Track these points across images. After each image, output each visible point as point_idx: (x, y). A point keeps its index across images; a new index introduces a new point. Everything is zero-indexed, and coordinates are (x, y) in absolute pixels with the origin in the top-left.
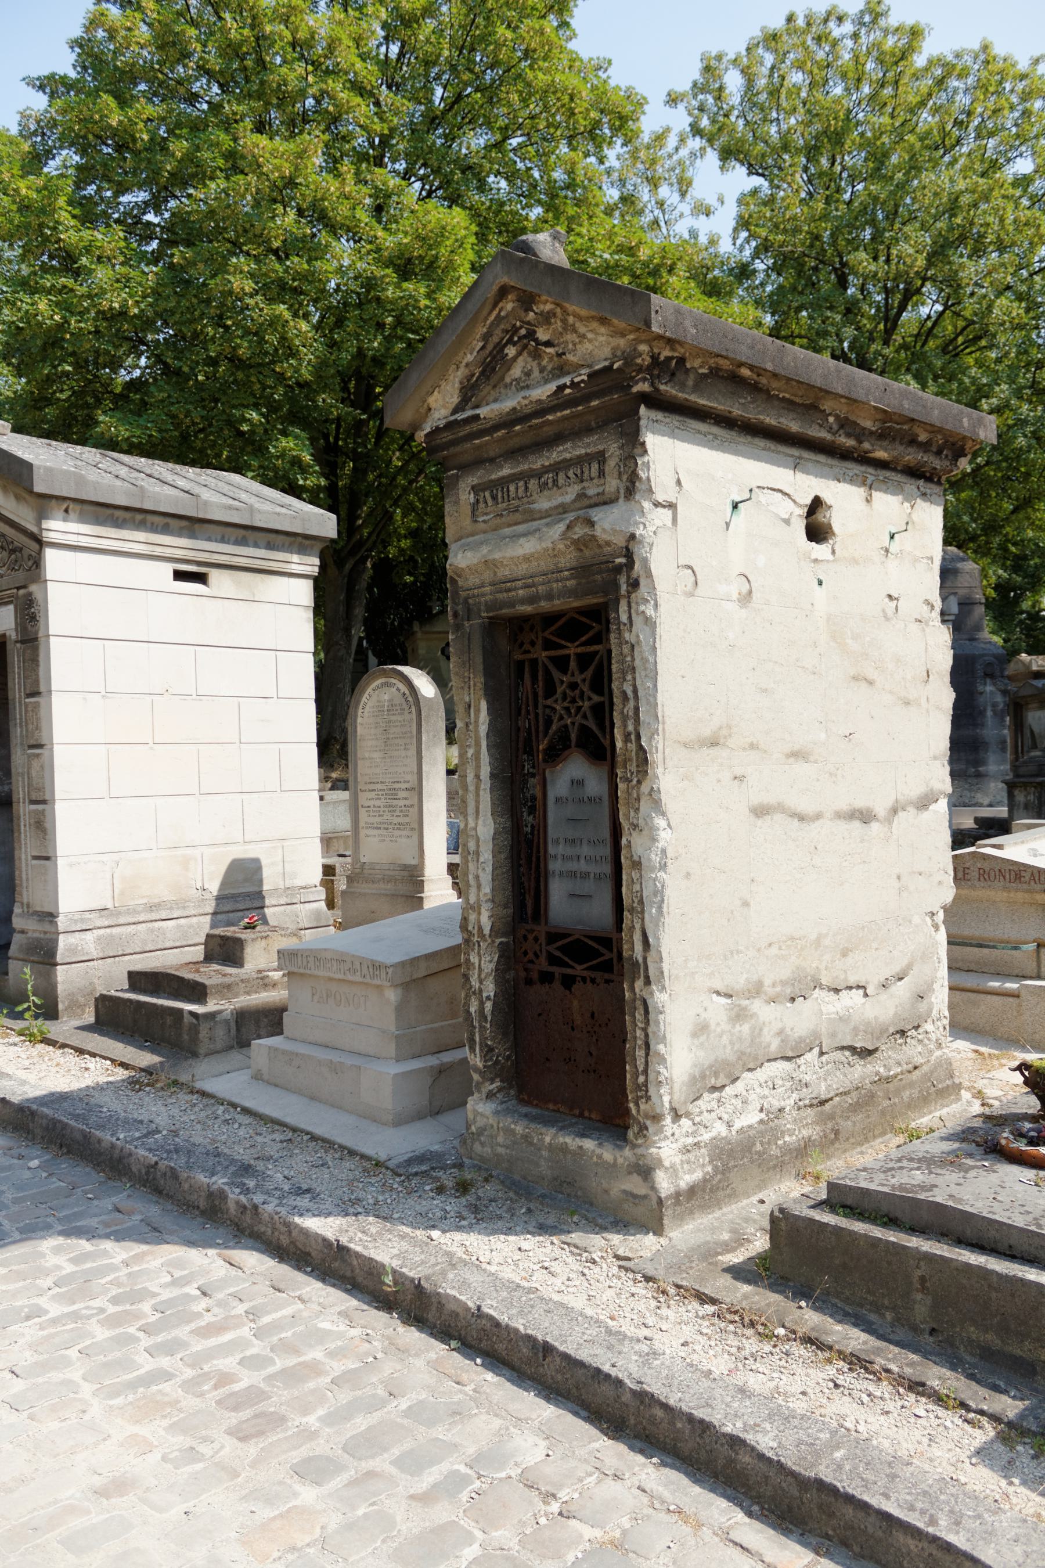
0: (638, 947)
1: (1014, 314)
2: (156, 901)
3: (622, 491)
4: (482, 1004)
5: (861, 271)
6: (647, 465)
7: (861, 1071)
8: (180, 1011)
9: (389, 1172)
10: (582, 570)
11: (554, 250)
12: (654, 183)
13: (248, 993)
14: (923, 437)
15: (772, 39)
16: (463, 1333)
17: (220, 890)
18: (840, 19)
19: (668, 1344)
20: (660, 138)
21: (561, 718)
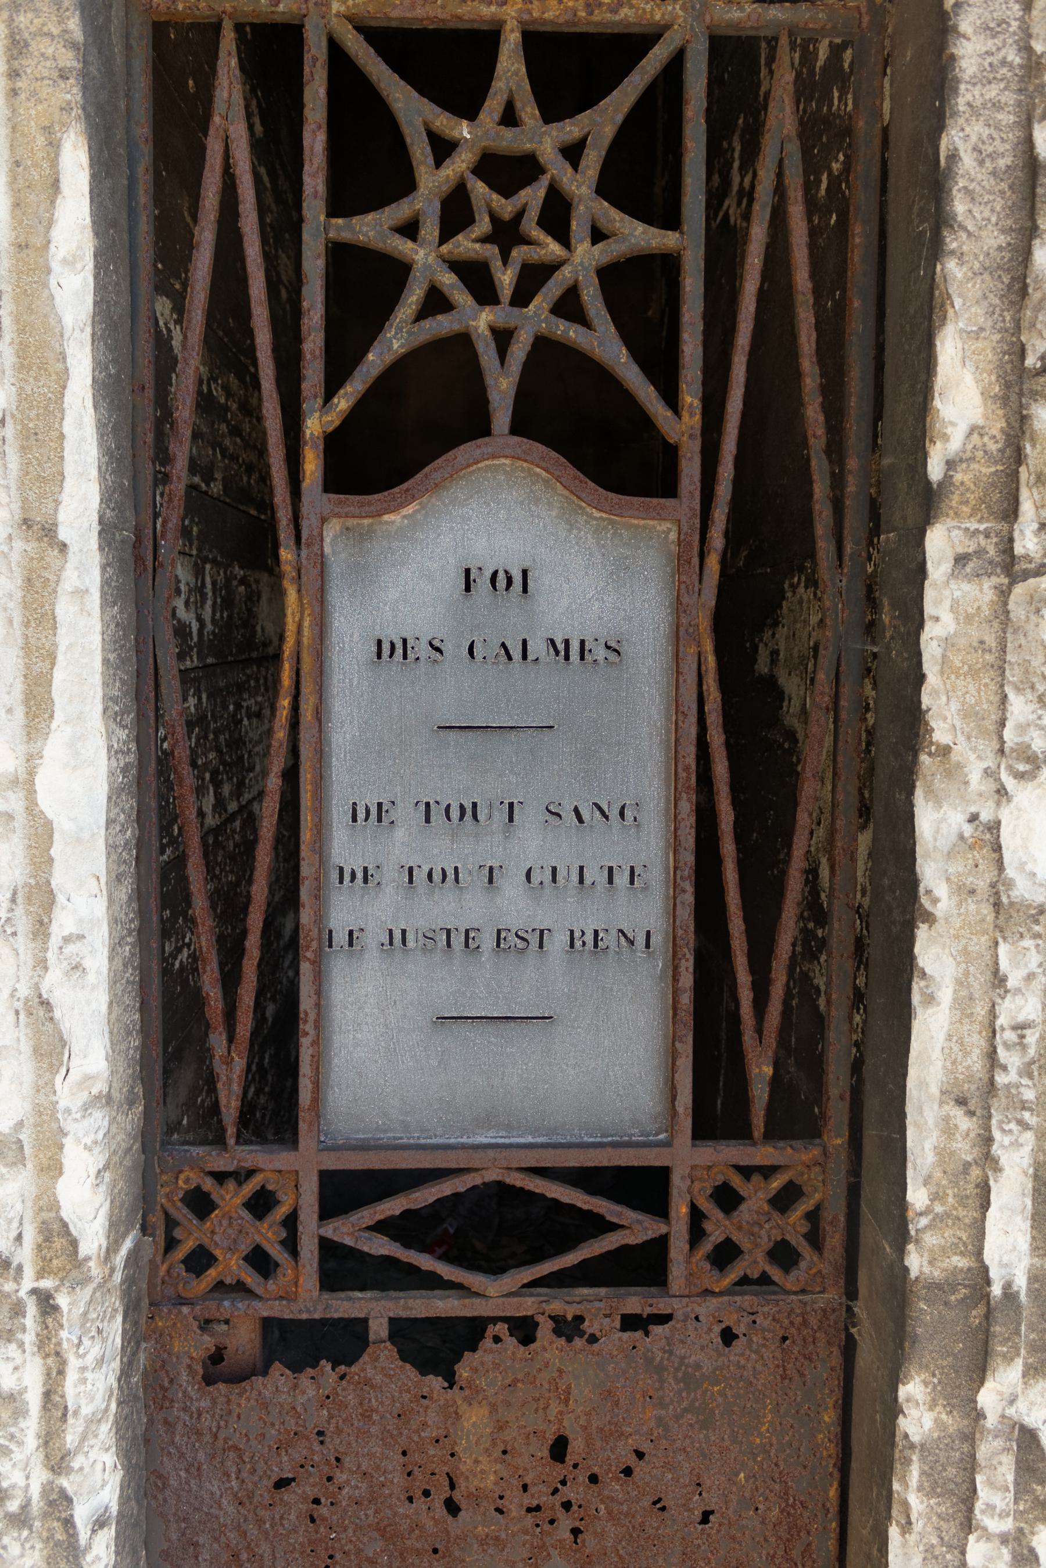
21: (436, 302)
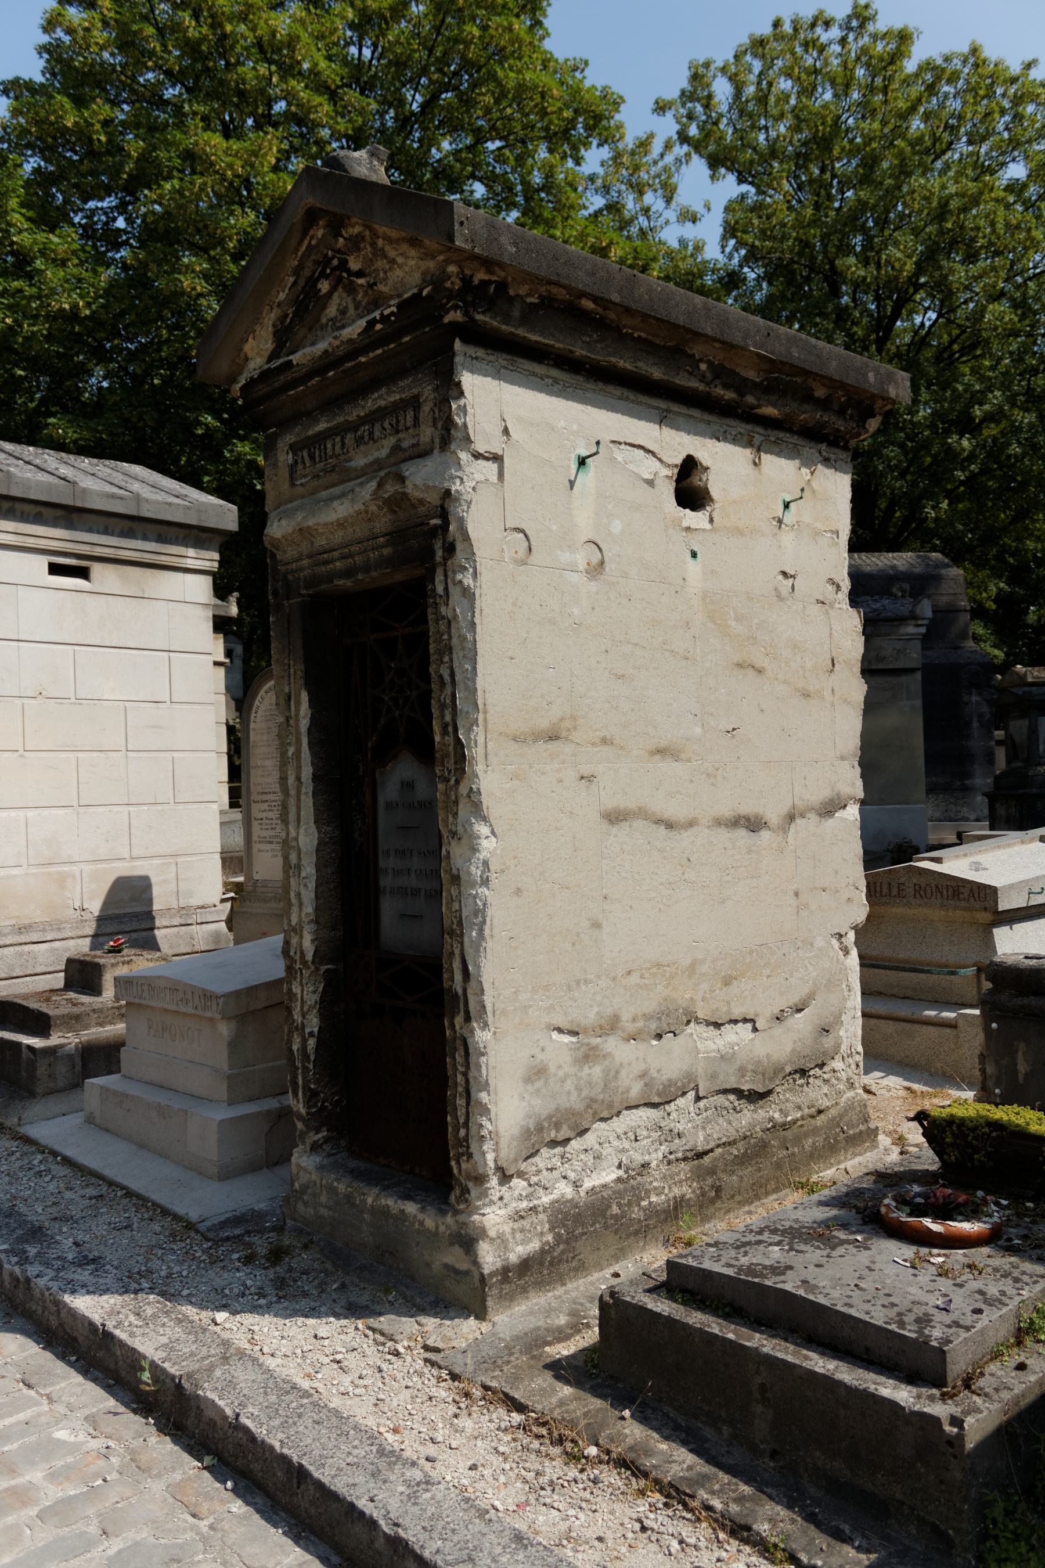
0: (458, 977)
1: (1007, 319)
2: (27, 922)
3: (437, 441)
4: (304, 1041)
5: (849, 276)
6: (464, 410)
7: (750, 1118)
8: (19, 1045)
9: (198, 1237)
10: (397, 535)
11: (372, 169)
12: (639, 190)
13: (101, 1025)
14: (820, 392)
15: (758, 45)
16: (220, 1446)
17: (102, 910)
18: (827, 24)
19: (452, 1470)
20: (644, 145)
